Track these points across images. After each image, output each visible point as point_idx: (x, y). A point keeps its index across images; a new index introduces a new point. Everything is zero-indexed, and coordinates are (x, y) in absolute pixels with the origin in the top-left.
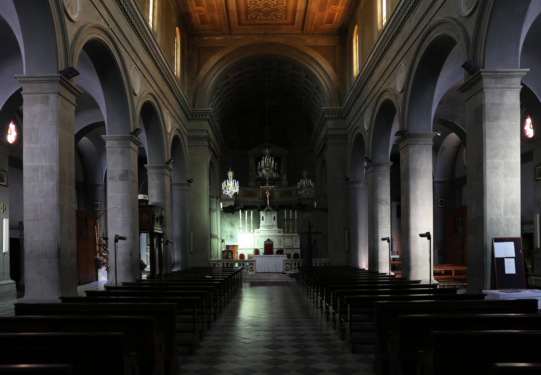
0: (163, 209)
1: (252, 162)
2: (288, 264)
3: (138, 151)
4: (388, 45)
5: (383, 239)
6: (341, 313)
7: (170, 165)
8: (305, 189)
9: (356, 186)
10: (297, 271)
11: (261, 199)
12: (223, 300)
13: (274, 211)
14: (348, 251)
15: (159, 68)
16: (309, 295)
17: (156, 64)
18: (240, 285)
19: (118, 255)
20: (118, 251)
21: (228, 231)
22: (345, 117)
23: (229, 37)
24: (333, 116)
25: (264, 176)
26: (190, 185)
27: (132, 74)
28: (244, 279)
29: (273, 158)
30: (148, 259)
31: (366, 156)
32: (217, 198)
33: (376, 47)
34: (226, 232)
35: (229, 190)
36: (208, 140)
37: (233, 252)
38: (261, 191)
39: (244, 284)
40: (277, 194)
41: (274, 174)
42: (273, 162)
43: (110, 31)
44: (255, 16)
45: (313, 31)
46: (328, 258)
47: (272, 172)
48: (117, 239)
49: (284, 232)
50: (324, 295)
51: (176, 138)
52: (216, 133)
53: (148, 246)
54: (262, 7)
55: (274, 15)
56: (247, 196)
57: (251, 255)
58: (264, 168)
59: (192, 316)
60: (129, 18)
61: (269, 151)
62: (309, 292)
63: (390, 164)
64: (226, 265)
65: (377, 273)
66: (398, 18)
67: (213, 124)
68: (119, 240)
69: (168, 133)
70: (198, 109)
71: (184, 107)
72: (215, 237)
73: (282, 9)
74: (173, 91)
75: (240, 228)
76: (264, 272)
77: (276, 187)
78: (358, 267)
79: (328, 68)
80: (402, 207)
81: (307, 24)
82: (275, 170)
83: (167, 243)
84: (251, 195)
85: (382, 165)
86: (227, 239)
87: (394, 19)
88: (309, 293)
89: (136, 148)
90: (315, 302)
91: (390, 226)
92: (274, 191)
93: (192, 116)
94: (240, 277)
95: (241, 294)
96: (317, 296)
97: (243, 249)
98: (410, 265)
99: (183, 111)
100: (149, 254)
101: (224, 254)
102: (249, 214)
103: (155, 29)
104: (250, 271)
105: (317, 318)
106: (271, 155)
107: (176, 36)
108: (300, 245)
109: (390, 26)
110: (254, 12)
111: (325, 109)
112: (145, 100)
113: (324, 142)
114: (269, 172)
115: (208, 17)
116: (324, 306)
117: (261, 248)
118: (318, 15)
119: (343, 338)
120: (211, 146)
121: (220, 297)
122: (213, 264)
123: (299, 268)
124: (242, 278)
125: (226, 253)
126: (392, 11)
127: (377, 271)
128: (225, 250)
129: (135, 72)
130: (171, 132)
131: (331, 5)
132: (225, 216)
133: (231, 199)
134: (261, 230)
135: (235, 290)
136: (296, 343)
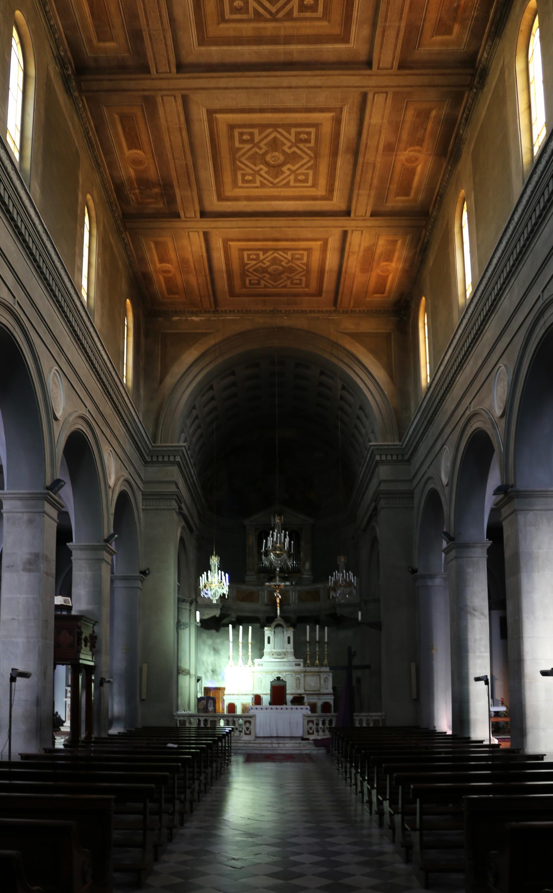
0: (96, 622)
1: (252, 540)
2: (312, 722)
3: (58, 518)
4: (476, 334)
5: (477, 679)
6: (404, 814)
7: (111, 544)
8: (342, 589)
9: (429, 583)
10: (327, 735)
11: (266, 605)
12: (197, 788)
13: (288, 627)
14: (417, 700)
15: (97, 371)
16: (349, 780)
17: (93, 364)
18: (227, 760)
19: (15, 703)
20: (16, 697)
21: (209, 662)
22: (409, 461)
23: (215, 317)
24: (389, 458)
25: (272, 564)
26: (144, 579)
27: (51, 381)
28: (235, 749)
29: (287, 533)
30: (68, 709)
31: (445, 530)
32: (191, 604)
33: (457, 337)
34: (205, 663)
35: (211, 590)
36: (177, 499)
37: (217, 700)
38: (266, 591)
39: (233, 758)
40: (293, 597)
41: (290, 562)
42: (287, 540)
43: (16, 307)
44: (257, 280)
45: (354, 307)
46: (381, 711)
47: (286, 557)
48: (14, 676)
49: (306, 664)
50: (374, 780)
51: (123, 496)
52: (191, 488)
53: (68, 686)
54: (268, 264)
55: (289, 278)
56: (243, 600)
57: (248, 706)
58: (272, 551)
59: (141, 817)
60: (49, 284)
61: (281, 519)
62: (348, 773)
63: (487, 545)
64: (204, 724)
65: (468, 740)
66: (492, 285)
67: (187, 470)
68: (18, 679)
69: (110, 487)
70: (162, 445)
71: (138, 441)
72: (186, 672)
73: (301, 268)
74: (120, 413)
75: (229, 657)
76: (270, 735)
77: (292, 584)
78: (434, 727)
79: (379, 373)
80: (509, 620)
81: (343, 293)
82: (291, 554)
83: (101, 682)
84: (250, 597)
85: (473, 547)
86: (206, 677)
87: (485, 288)
88: (348, 776)
89: (54, 513)
90: (358, 791)
91: (488, 654)
92: (289, 591)
93: (152, 456)
94: (227, 745)
95: (229, 777)
96: (362, 783)
97: (233, 695)
98: (525, 725)
99: (136, 447)
100: (69, 701)
101: (201, 703)
102: (246, 632)
103: (92, 302)
104: (246, 734)
105: (362, 821)
106: (284, 528)
107: (125, 315)
108: (334, 688)
109: (479, 300)
110: (255, 273)
111: (374, 446)
112: (73, 429)
113: (374, 504)
114: (280, 557)
115: (179, 281)
116: (374, 799)
117: (265, 692)
118: (360, 278)
119: (408, 860)
120: (182, 511)
121: (191, 781)
122: (180, 721)
123: (330, 730)
124: (230, 747)
125: (204, 702)
126: (480, 272)
127: (466, 736)
128: (203, 696)
129: (56, 378)
130: (115, 484)
131: (381, 262)
132: (205, 634)
133: (216, 606)
134: (265, 662)
135: (219, 769)
136: (324, 869)
